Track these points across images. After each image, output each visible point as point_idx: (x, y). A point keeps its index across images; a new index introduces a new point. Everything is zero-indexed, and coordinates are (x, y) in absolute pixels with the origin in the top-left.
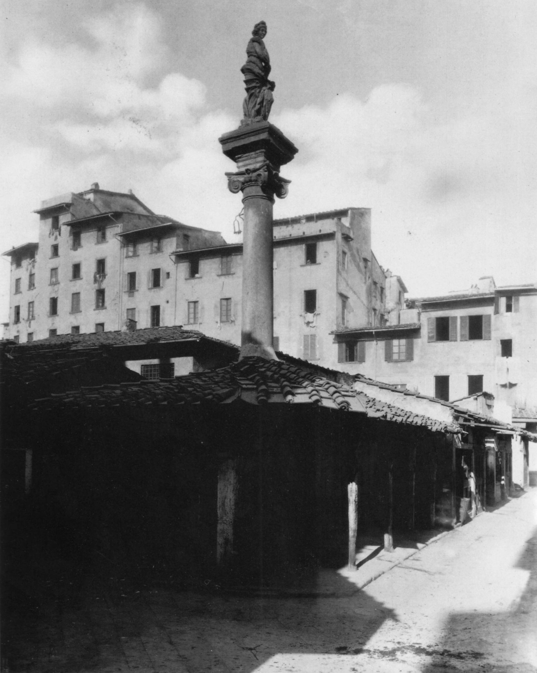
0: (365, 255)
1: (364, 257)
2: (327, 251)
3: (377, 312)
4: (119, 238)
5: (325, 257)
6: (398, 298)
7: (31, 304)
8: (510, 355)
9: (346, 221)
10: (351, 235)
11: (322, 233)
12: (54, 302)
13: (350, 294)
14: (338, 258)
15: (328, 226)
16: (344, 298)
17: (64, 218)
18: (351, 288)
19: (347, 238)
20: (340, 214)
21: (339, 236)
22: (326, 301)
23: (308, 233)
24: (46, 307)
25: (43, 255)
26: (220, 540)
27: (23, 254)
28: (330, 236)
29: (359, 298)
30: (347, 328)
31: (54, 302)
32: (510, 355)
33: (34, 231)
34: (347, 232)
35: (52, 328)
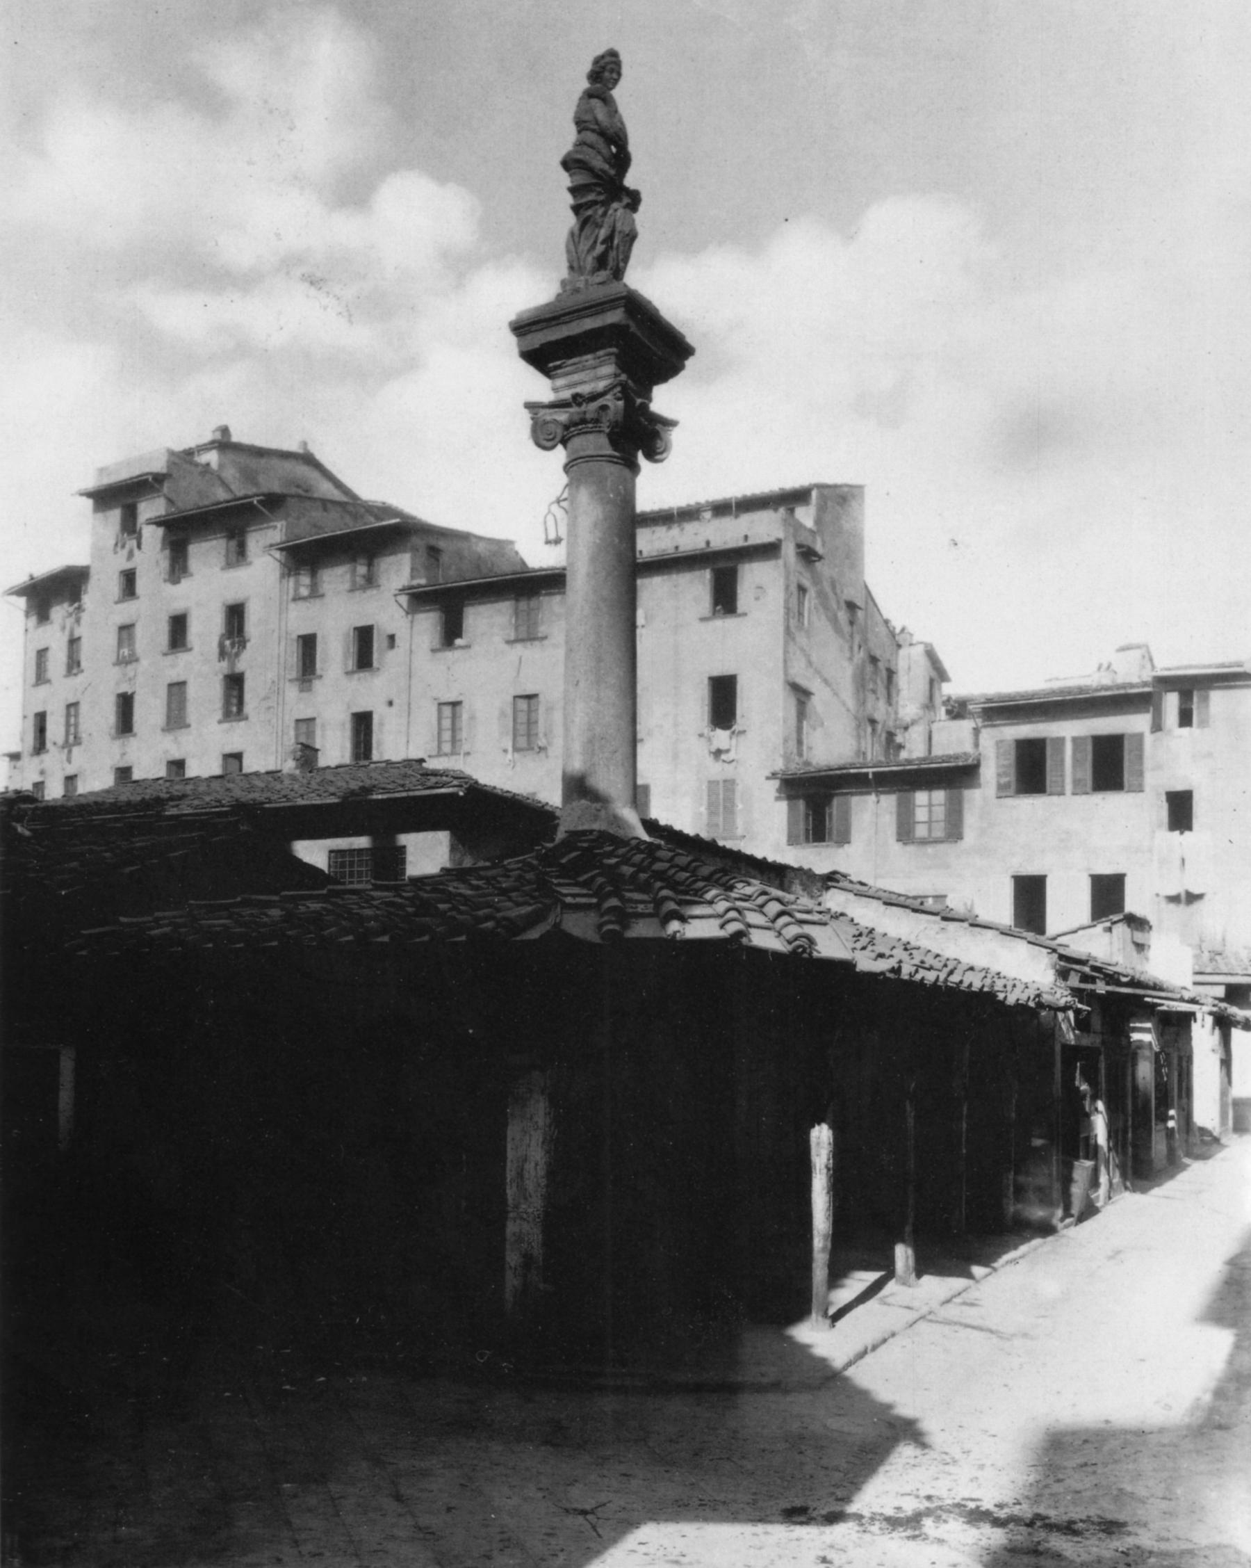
0: (850, 593)
1: (849, 598)
2: (762, 585)
3: (879, 727)
4: (278, 555)
5: (757, 599)
6: (927, 693)
7: (72, 707)
8: (1189, 827)
9: (806, 516)
10: (819, 548)
11: (751, 542)
12: (126, 704)
13: (814, 685)
14: (786, 601)
15: (763, 527)
16: (801, 694)
17: (150, 509)
18: (818, 672)
19: (808, 555)
20: (793, 498)
21: (789, 550)
22: (760, 702)
23: (718, 543)
24: (108, 714)
25: (100, 594)
26: (513, 1258)
27: (53, 592)
28: (768, 551)
29: (836, 694)
30: (807, 763)
31: (126, 704)
32: (1189, 827)
33: (78, 538)
34: (808, 541)
35: (122, 764)
